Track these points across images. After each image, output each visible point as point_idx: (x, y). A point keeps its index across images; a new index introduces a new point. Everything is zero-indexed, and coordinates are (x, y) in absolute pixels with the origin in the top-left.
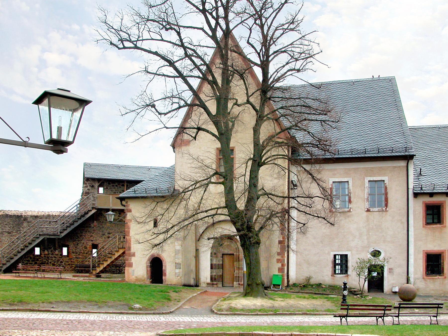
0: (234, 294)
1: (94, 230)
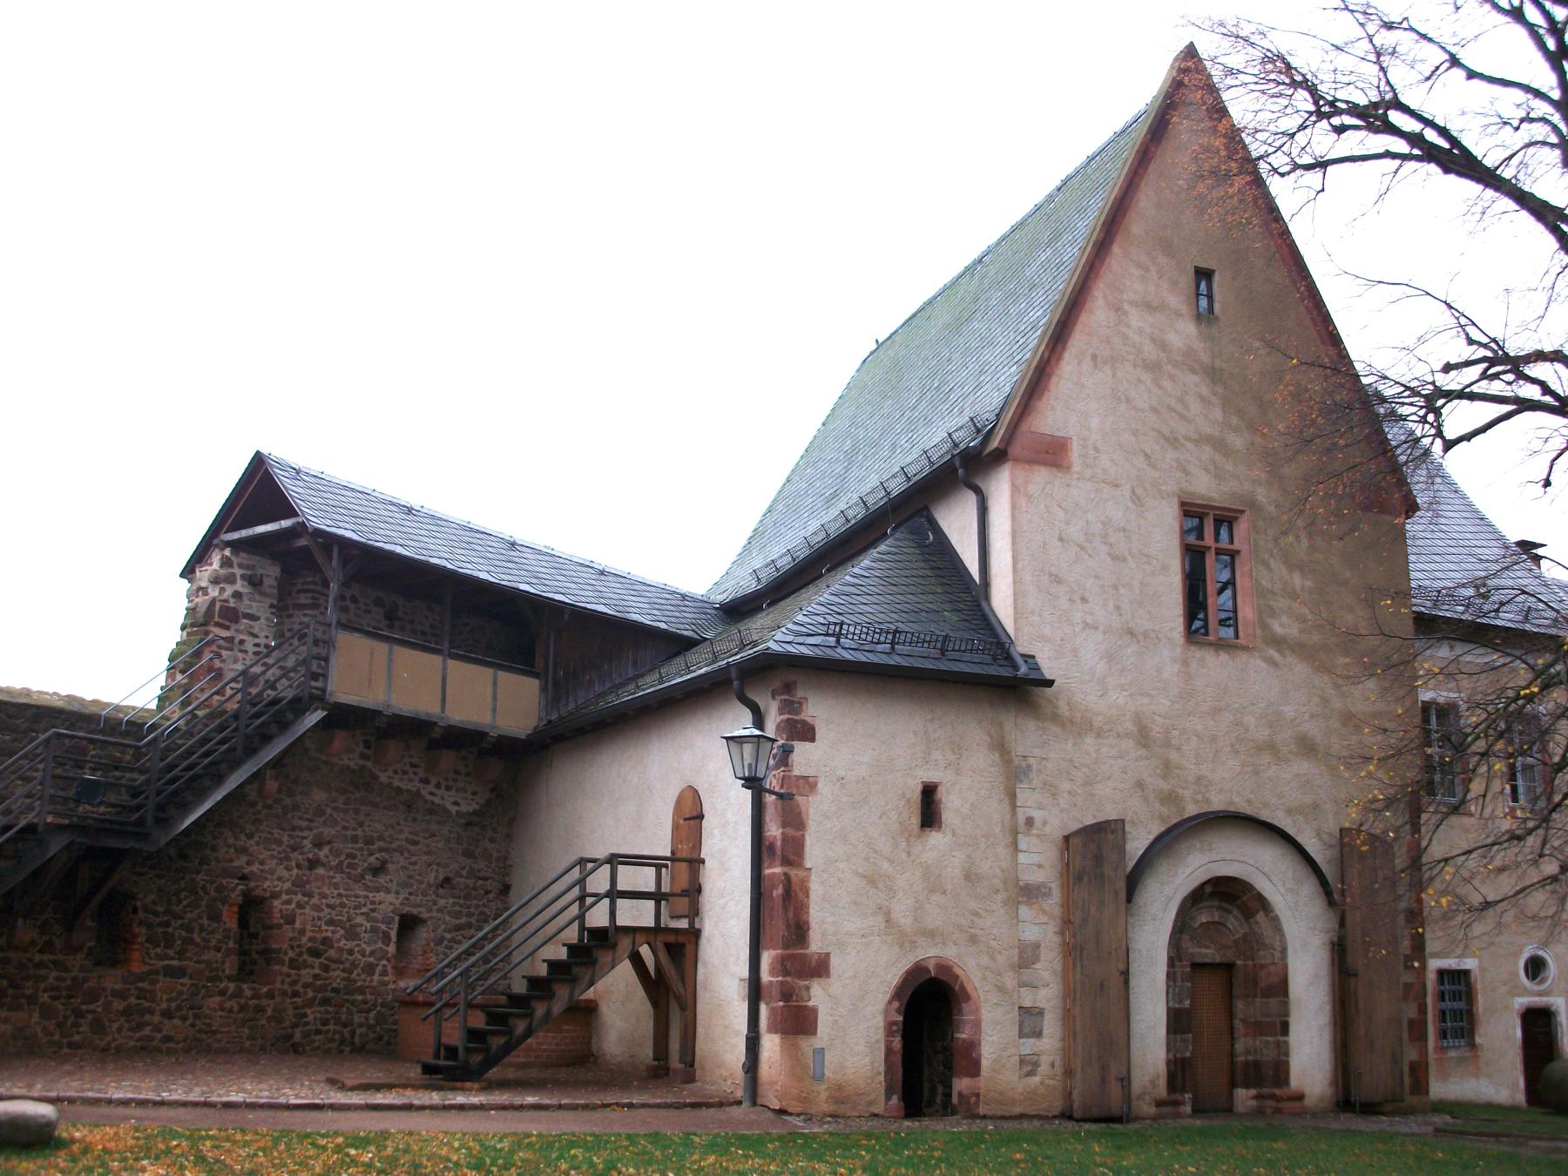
1: (254, 822)
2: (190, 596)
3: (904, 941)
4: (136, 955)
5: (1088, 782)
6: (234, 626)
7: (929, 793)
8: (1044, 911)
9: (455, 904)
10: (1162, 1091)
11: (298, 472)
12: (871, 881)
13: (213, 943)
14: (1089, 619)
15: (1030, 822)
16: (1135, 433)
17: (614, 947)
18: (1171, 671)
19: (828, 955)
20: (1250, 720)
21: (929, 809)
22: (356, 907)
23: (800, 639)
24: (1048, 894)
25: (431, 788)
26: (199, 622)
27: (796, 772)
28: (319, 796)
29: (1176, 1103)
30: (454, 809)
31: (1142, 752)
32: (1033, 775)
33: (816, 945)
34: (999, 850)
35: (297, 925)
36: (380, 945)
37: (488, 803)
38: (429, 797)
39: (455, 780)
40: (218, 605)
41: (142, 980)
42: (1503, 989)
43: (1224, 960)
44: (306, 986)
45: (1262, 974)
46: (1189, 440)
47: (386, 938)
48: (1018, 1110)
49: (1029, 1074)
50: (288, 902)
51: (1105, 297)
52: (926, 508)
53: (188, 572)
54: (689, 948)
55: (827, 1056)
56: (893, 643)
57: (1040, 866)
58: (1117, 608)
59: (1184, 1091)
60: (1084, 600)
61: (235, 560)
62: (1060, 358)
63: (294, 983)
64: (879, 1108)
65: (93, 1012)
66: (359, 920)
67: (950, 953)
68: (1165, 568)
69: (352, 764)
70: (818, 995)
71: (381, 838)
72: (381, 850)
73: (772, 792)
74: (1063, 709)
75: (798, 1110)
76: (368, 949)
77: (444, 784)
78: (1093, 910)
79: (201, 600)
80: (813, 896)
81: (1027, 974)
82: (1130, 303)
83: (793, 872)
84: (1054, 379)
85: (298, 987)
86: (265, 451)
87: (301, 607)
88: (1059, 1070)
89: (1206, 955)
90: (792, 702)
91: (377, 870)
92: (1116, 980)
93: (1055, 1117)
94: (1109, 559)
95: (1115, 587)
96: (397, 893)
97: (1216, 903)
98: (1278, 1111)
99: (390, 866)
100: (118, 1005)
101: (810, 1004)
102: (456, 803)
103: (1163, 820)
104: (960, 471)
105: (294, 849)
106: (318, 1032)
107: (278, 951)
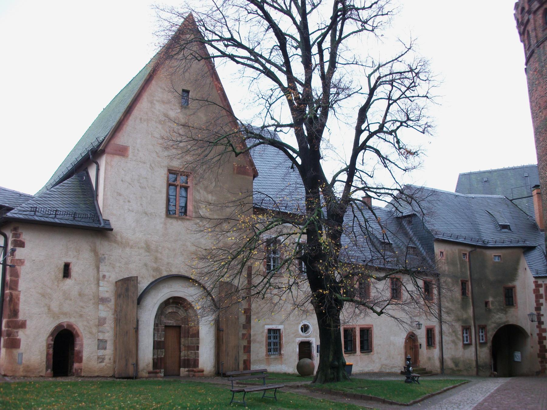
3: (55, 316)
5: (126, 264)
8: (108, 307)
10: (151, 368)
12: (43, 295)
14: (130, 208)
15: (104, 276)
16: (153, 145)
18: (160, 227)
19: (25, 321)
20: (189, 244)
21: (67, 271)
23: (20, 213)
24: (110, 301)
27: (17, 258)
29: (156, 373)
31: (148, 254)
33: (21, 317)
34: (92, 286)
42: (292, 335)
43: (177, 325)
45: (191, 330)
48: (96, 374)
49: (101, 362)
51: (147, 99)
52: (87, 168)
55: (24, 356)
56: (56, 214)
57: (107, 291)
59: (161, 368)
60: (129, 201)
62: (128, 119)
64: (43, 374)
68: (160, 192)
70: (21, 334)
74: (119, 238)
75: (11, 375)
78: (124, 307)
80: (21, 300)
81: (101, 328)
82: (157, 101)
83: (14, 292)
84: (125, 126)
88: (112, 361)
89: (170, 323)
90: (16, 234)
92: (132, 331)
93: (110, 377)
94: (139, 188)
95: (141, 198)
97: (175, 305)
98: (194, 376)
101: (18, 337)
103: (153, 277)
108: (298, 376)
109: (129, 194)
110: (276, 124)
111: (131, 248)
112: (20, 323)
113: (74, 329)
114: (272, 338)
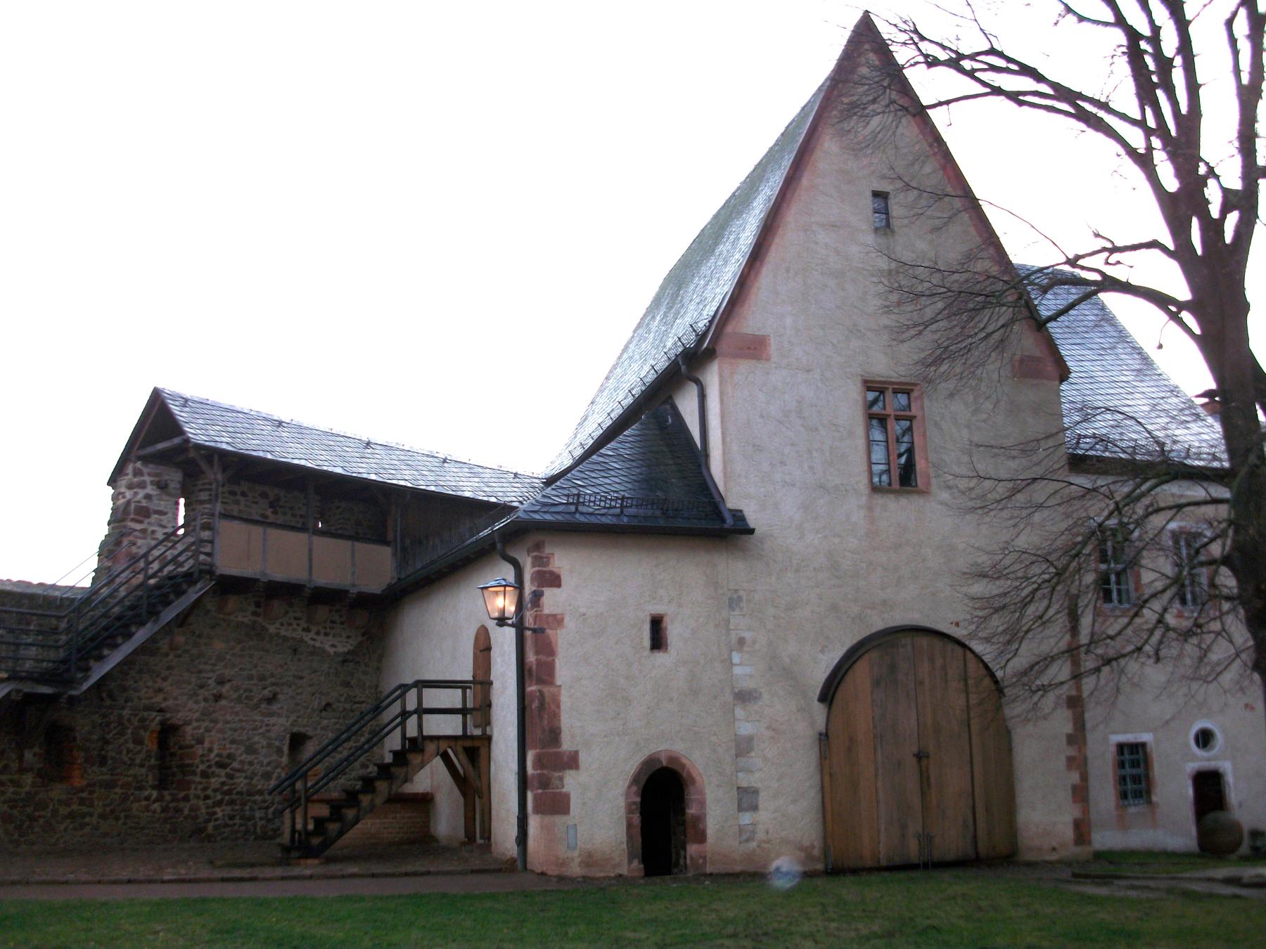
0: (1194, 892)
2: (114, 498)
4: (77, 773)
6: (146, 521)
7: (657, 624)
9: (335, 723)
11: (186, 400)
13: (138, 761)
14: (787, 478)
15: (741, 641)
17: (422, 751)
18: (859, 516)
19: (576, 753)
22: (254, 729)
23: (545, 509)
25: (312, 635)
26: (118, 518)
27: (546, 611)
28: (219, 645)
30: (332, 651)
32: (743, 604)
33: (566, 745)
35: (206, 745)
36: (275, 757)
37: (360, 644)
38: (311, 642)
39: (332, 628)
40: (133, 506)
41: (83, 791)
44: (215, 791)
46: (869, 329)
47: (279, 751)
50: (198, 728)
52: (671, 397)
53: (112, 482)
54: (483, 751)
57: (751, 676)
58: (811, 468)
61: (145, 470)
63: (205, 789)
64: (624, 871)
65: (44, 817)
66: (256, 739)
67: (679, 748)
69: (246, 620)
70: (572, 783)
71: (272, 675)
72: (273, 684)
73: (529, 629)
76: (266, 761)
77: (322, 631)
79: (121, 501)
80: (563, 707)
81: (742, 761)
83: (546, 690)
85: (209, 792)
86: (160, 386)
87: (202, 502)
90: (541, 558)
91: (272, 699)
96: (288, 717)
99: (280, 696)
100: (63, 811)
101: (564, 790)
102: (333, 646)
104: (683, 368)
105: (201, 687)
106: (226, 825)
107: (191, 765)
108: (1198, 856)
109: (775, 442)
110: (1109, 246)
111: (797, 571)
112: (565, 759)
113: (683, 766)
114: (1127, 765)
